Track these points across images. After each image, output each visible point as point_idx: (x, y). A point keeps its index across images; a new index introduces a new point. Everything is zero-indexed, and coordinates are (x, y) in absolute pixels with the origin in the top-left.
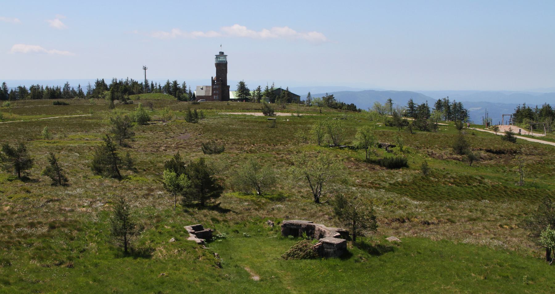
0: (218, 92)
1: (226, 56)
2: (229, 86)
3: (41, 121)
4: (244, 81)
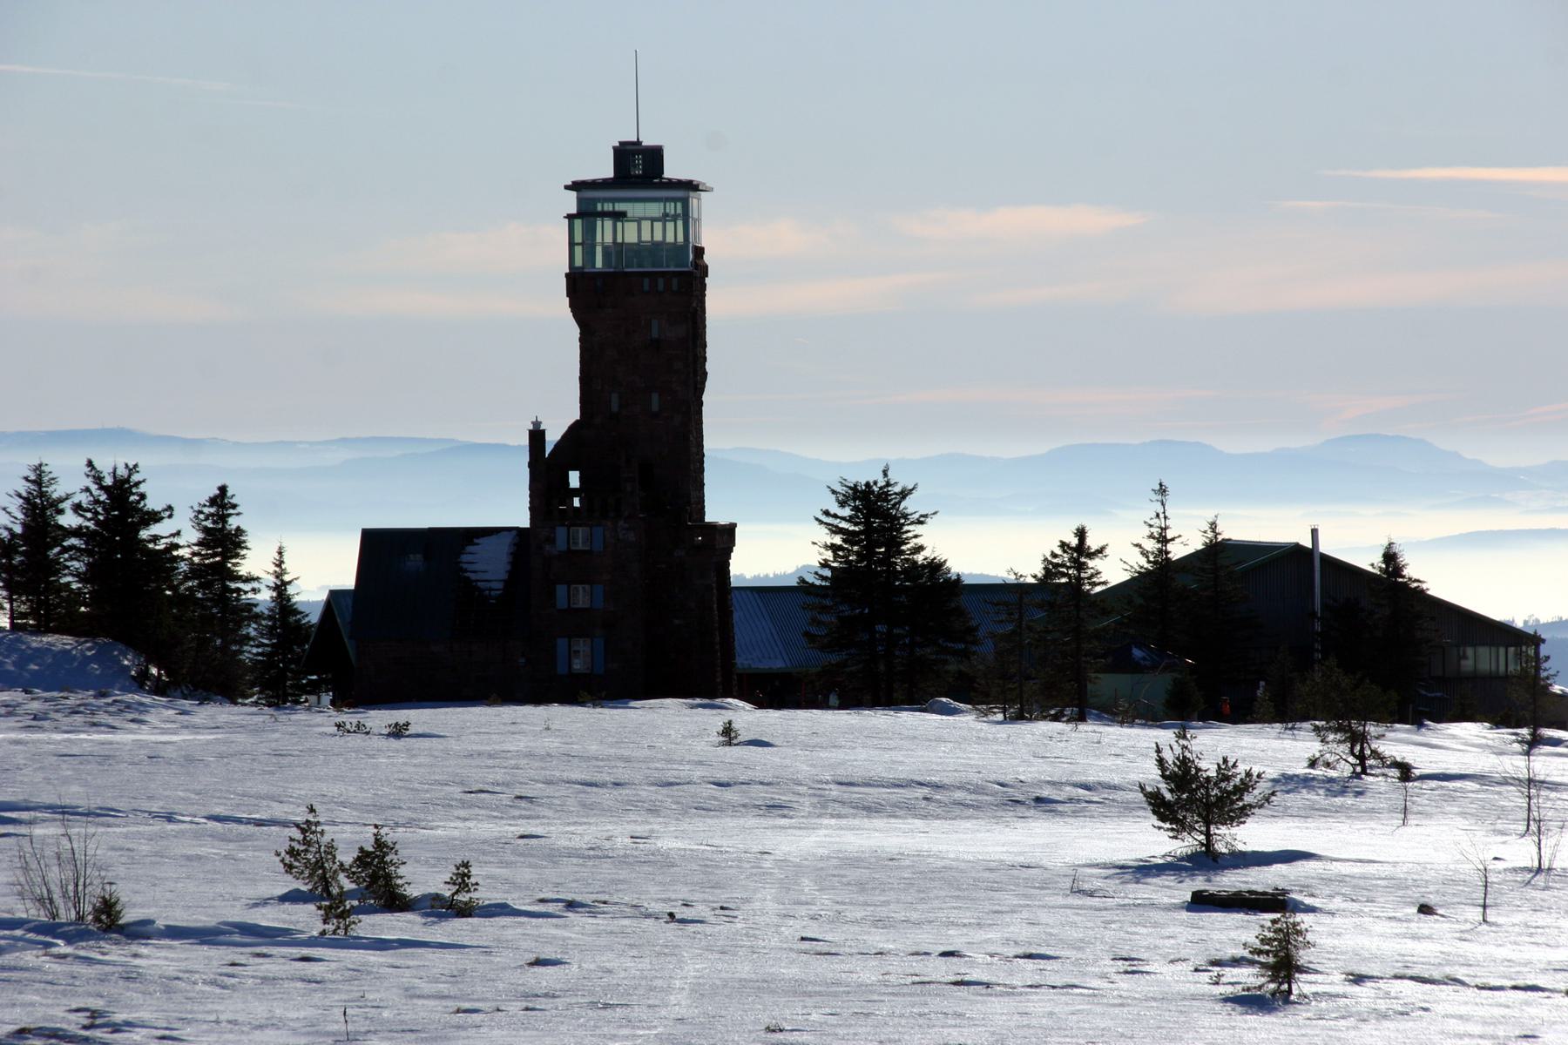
1: (691, 186)
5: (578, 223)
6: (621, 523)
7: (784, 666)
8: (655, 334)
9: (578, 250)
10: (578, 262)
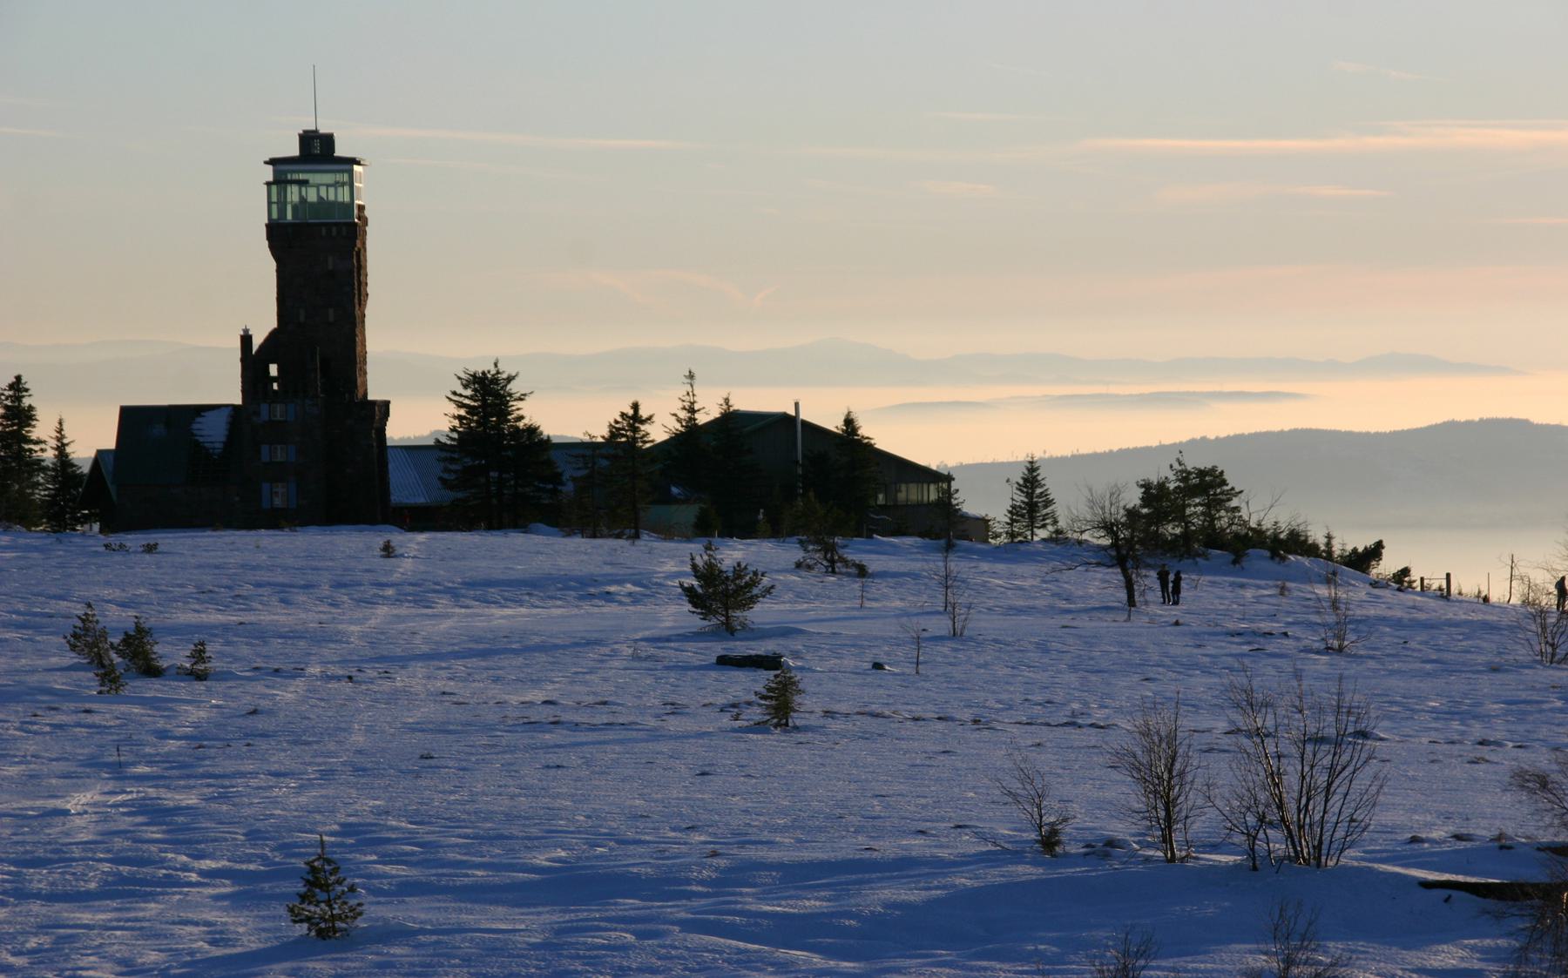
0: (265, 457)
2: (131, 418)
3: (999, 885)
4: (507, 369)
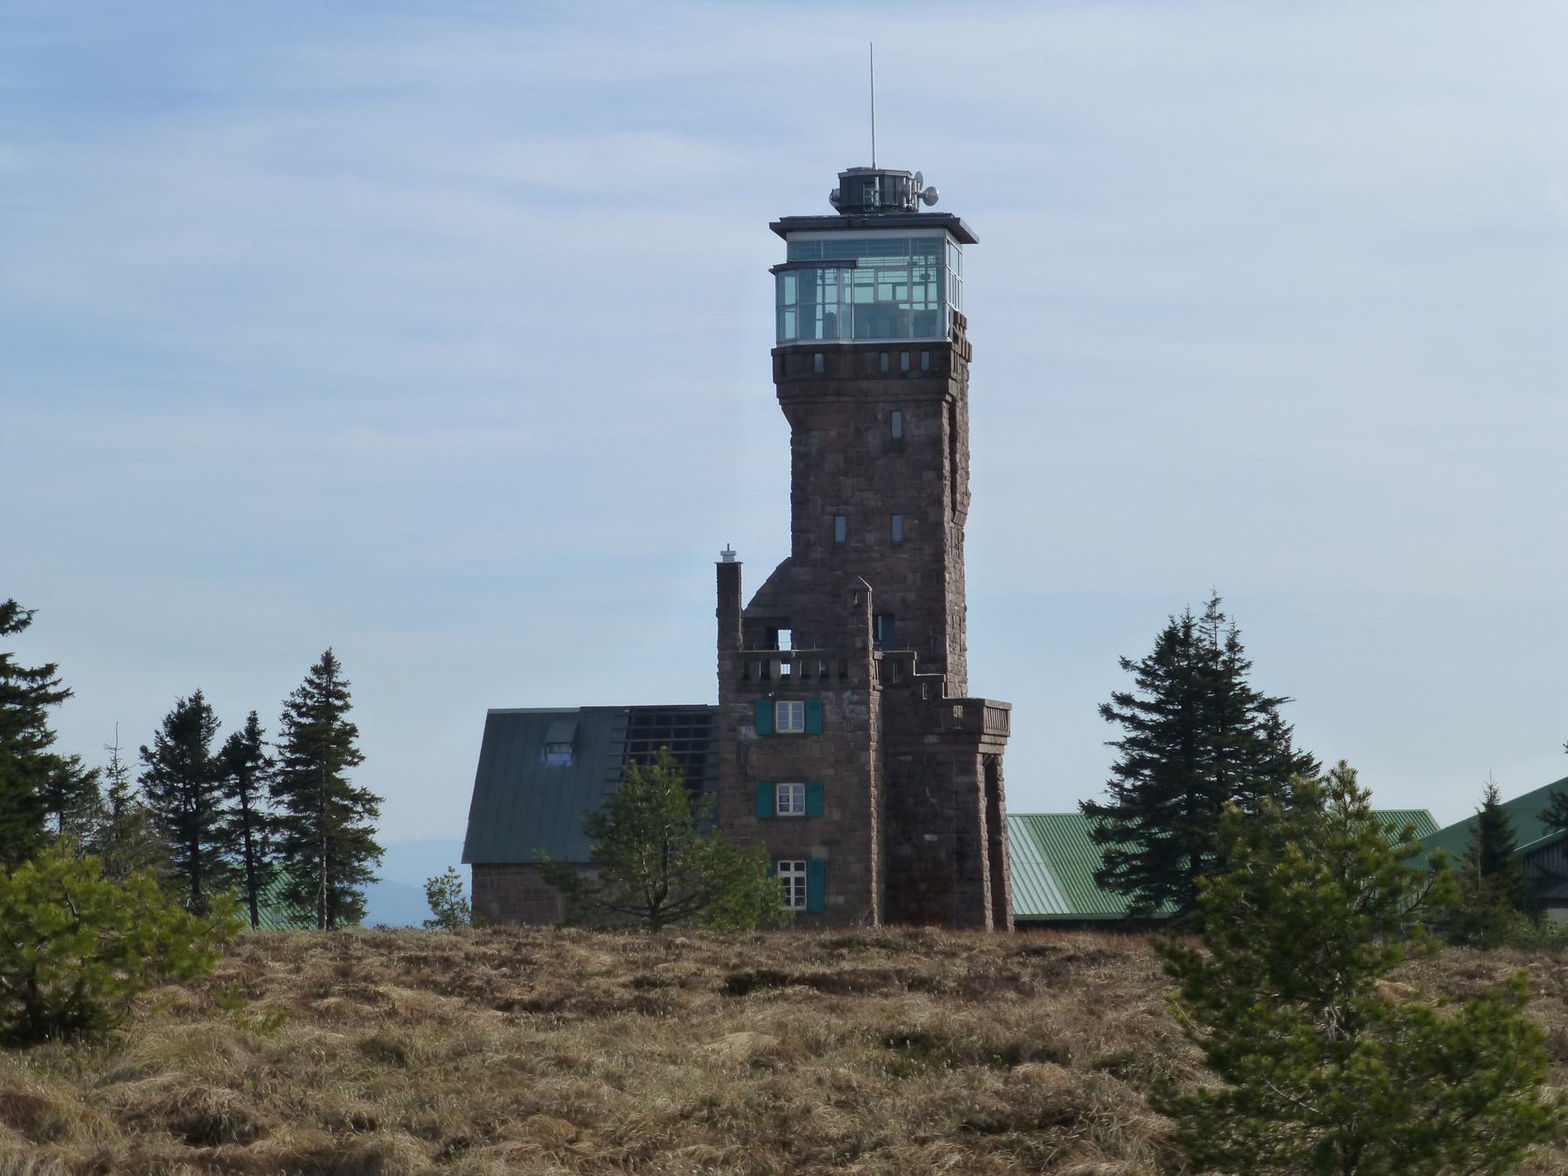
5: (790, 282)
6: (847, 694)
7: (1076, 912)
8: (897, 432)
9: (790, 318)
10: (790, 333)
